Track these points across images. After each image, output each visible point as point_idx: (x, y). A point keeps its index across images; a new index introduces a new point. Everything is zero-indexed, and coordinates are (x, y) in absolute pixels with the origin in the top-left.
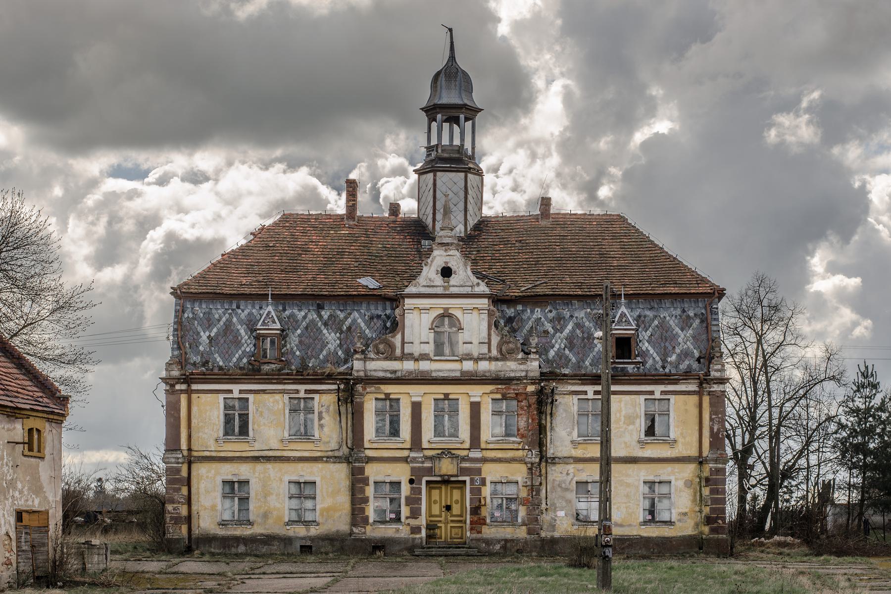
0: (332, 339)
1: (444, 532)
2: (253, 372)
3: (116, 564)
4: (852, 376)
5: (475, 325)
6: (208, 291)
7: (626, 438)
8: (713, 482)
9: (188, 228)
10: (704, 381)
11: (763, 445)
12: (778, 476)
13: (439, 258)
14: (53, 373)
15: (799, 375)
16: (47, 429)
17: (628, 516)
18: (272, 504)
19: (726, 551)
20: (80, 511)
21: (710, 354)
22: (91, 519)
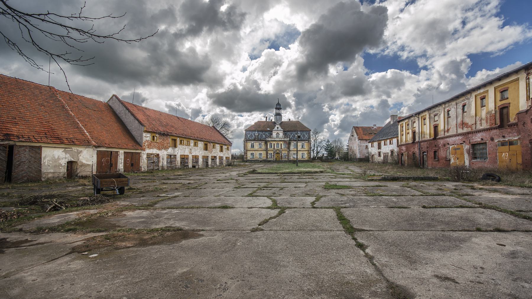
0: (264, 136)
1: (277, 159)
2: (254, 140)
3: (238, 163)
4: (326, 140)
5: (281, 134)
6: (250, 130)
7: (299, 148)
8: (310, 153)
9: (248, 123)
10: (309, 141)
11: (316, 149)
12: (318, 153)
13: (277, 126)
14: (230, 140)
15: (320, 140)
16: (230, 147)
17: (300, 157)
18: (257, 155)
19: (312, 162)
20: (233, 157)
21: (309, 138)
22: (235, 158)
